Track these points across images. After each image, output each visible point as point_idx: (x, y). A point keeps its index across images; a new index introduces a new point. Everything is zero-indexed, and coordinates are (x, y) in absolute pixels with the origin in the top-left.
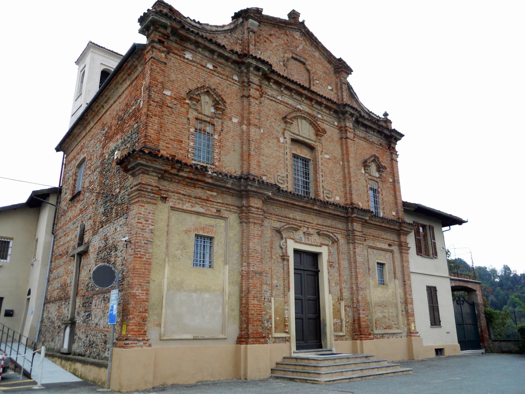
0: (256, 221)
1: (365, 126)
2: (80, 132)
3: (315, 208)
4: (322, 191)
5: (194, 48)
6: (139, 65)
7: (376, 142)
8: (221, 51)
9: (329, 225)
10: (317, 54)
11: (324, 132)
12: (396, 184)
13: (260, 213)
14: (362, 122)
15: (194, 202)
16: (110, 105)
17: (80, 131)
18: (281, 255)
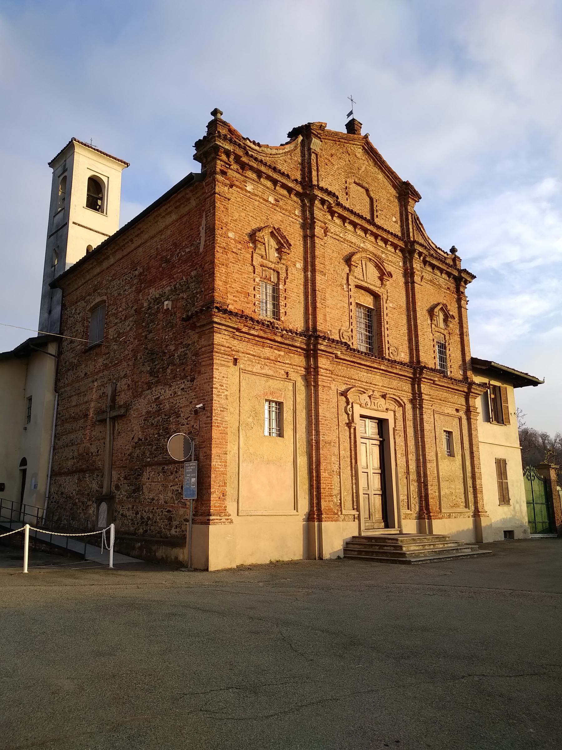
1: (433, 267)
2: (92, 268)
3: (382, 368)
5: (256, 178)
6: (193, 198)
7: (443, 286)
8: (284, 181)
9: (395, 387)
10: (381, 176)
11: (390, 275)
12: (465, 337)
13: (328, 375)
14: (429, 262)
15: (263, 363)
16: (143, 241)
17: (91, 266)
18: (347, 422)
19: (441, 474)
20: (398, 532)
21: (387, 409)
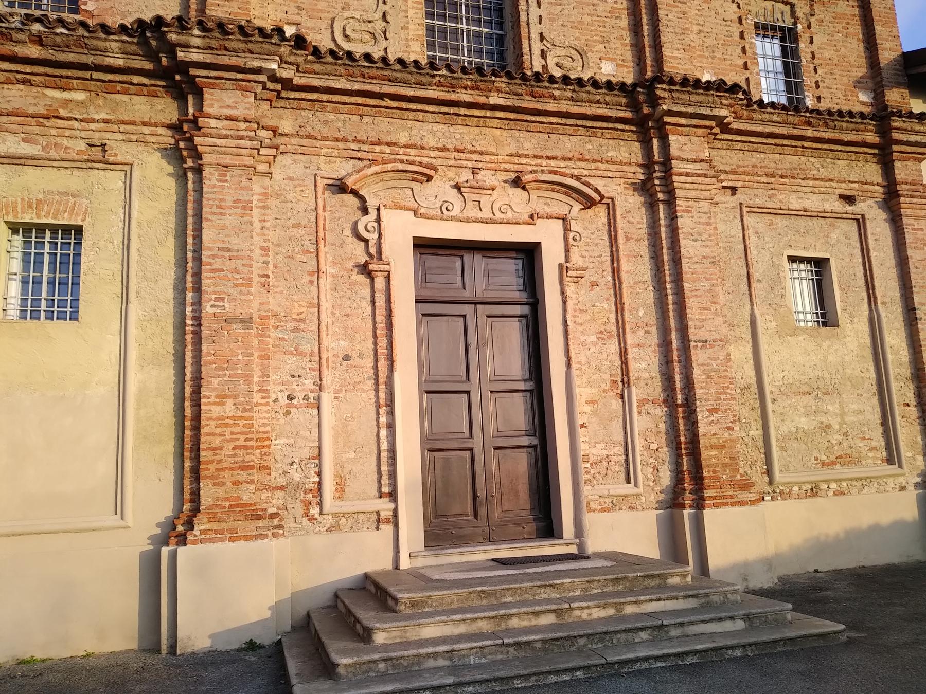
0: (227, 160)
3: (494, 100)
4: (536, 52)
19: (766, 380)
20: (573, 550)
21: (532, 217)
